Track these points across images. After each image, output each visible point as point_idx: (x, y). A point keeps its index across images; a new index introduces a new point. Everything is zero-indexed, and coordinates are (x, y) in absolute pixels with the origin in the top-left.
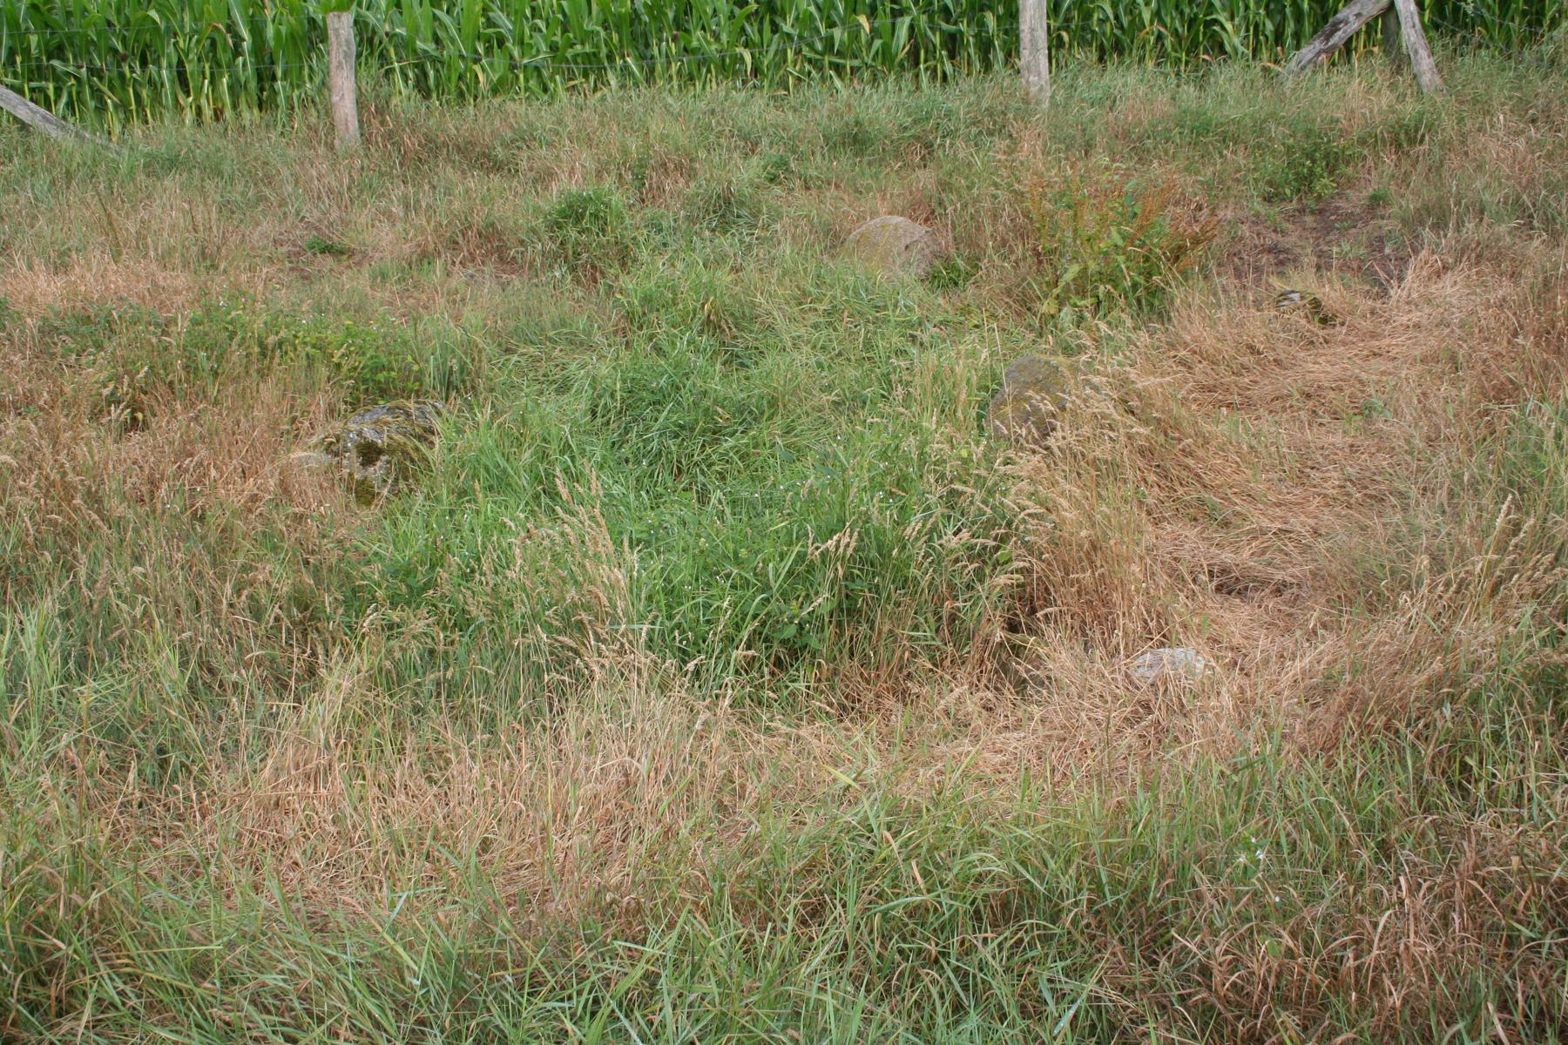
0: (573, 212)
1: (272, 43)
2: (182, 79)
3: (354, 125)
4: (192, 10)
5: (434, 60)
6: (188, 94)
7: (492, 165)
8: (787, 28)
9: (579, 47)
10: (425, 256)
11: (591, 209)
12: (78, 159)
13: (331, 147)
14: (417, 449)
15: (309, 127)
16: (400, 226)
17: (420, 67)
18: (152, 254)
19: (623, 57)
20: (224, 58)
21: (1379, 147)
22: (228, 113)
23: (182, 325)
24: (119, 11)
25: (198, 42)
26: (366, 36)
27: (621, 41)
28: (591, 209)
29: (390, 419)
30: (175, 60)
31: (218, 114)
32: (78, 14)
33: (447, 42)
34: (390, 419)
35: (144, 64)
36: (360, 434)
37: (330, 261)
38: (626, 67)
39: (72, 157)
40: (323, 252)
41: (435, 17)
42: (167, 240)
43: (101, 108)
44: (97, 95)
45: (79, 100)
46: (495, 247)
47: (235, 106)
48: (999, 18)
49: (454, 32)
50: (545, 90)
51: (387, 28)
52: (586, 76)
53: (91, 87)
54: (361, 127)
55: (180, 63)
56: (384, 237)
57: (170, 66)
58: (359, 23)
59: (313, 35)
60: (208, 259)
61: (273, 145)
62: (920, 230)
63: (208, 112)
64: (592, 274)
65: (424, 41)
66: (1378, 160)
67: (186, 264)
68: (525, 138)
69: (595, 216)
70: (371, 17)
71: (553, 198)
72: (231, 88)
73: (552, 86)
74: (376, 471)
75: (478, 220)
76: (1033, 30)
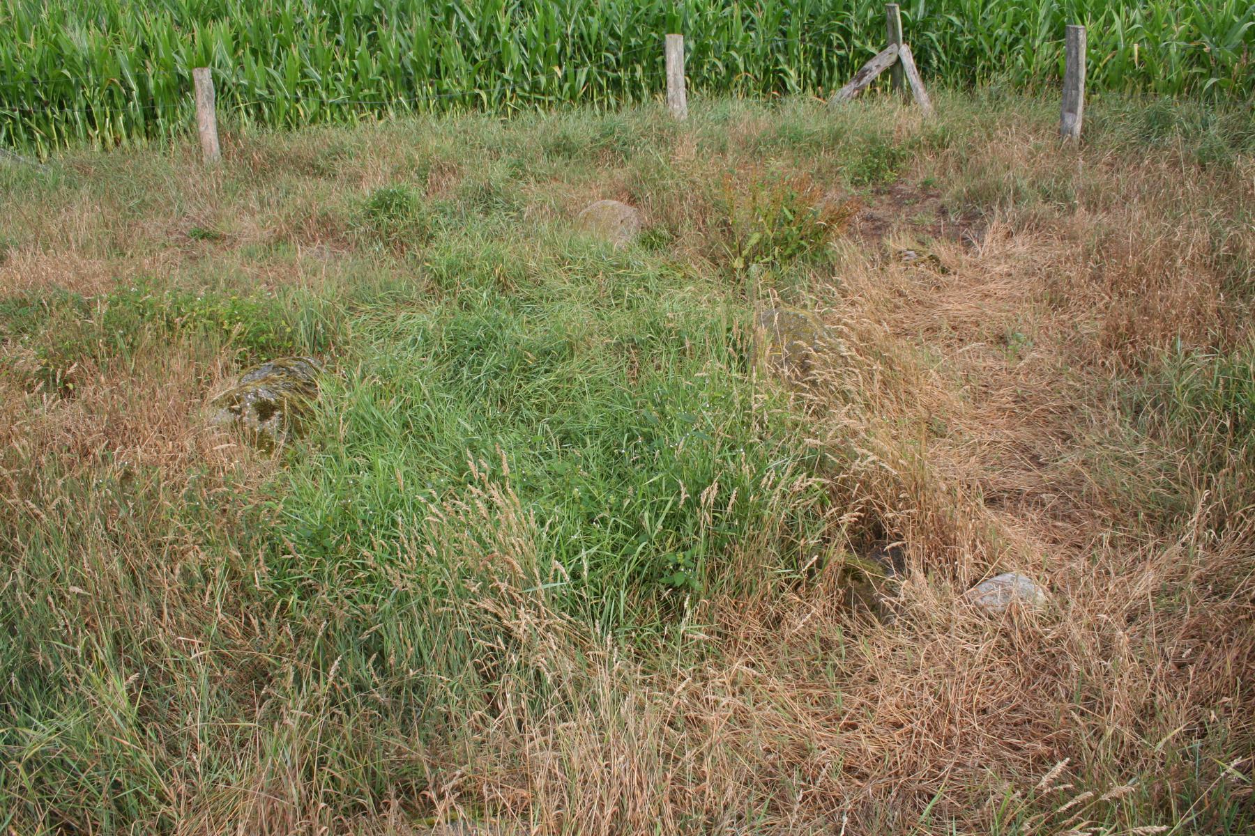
0: (383, 203)
1: (153, 92)
2: (90, 118)
3: (216, 146)
4: (94, 70)
5: (268, 102)
6: (95, 128)
7: (315, 170)
8: (506, 76)
9: (366, 91)
10: (280, 239)
11: (396, 201)
12: (15, 174)
13: (200, 162)
14: (302, 402)
15: (184, 149)
16: (258, 217)
17: (259, 108)
18: (74, 246)
19: (397, 97)
20: (119, 102)
21: (922, 149)
22: (125, 142)
23: (101, 309)
24: (40, 71)
25: (100, 92)
26: (221, 87)
27: (395, 86)
28: (396, 201)
29: (275, 376)
30: (84, 105)
31: (117, 142)
32: (9, 73)
33: (276, 91)
34: (275, 376)
35: (61, 107)
36: (256, 395)
37: (208, 246)
38: (399, 102)
39: (10, 173)
40: (202, 238)
41: (268, 73)
42: (83, 234)
43: (31, 140)
44: (28, 130)
45: (15, 134)
46: (329, 229)
47: (129, 136)
48: (644, 69)
49: (281, 82)
50: (345, 120)
51: (234, 80)
52: (372, 110)
53: (23, 125)
54: (221, 148)
55: (88, 107)
56: (250, 227)
57: (80, 108)
58: (215, 78)
59: (184, 86)
60: (118, 248)
61: (160, 162)
62: (630, 211)
63: (110, 141)
64: (399, 247)
65: (260, 89)
66: (922, 160)
67: (101, 253)
68: (338, 152)
69: (399, 206)
70: (223, 74)
71: (366, 192)
72: (125, 124)
73: (349, 117)
74: (272, 424)
75: (316, 211)
76: (675, 74)
